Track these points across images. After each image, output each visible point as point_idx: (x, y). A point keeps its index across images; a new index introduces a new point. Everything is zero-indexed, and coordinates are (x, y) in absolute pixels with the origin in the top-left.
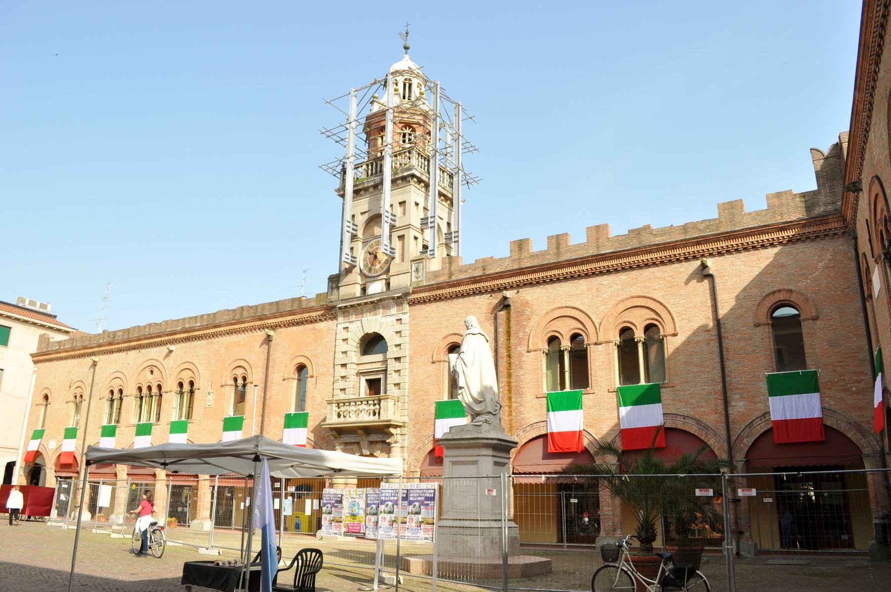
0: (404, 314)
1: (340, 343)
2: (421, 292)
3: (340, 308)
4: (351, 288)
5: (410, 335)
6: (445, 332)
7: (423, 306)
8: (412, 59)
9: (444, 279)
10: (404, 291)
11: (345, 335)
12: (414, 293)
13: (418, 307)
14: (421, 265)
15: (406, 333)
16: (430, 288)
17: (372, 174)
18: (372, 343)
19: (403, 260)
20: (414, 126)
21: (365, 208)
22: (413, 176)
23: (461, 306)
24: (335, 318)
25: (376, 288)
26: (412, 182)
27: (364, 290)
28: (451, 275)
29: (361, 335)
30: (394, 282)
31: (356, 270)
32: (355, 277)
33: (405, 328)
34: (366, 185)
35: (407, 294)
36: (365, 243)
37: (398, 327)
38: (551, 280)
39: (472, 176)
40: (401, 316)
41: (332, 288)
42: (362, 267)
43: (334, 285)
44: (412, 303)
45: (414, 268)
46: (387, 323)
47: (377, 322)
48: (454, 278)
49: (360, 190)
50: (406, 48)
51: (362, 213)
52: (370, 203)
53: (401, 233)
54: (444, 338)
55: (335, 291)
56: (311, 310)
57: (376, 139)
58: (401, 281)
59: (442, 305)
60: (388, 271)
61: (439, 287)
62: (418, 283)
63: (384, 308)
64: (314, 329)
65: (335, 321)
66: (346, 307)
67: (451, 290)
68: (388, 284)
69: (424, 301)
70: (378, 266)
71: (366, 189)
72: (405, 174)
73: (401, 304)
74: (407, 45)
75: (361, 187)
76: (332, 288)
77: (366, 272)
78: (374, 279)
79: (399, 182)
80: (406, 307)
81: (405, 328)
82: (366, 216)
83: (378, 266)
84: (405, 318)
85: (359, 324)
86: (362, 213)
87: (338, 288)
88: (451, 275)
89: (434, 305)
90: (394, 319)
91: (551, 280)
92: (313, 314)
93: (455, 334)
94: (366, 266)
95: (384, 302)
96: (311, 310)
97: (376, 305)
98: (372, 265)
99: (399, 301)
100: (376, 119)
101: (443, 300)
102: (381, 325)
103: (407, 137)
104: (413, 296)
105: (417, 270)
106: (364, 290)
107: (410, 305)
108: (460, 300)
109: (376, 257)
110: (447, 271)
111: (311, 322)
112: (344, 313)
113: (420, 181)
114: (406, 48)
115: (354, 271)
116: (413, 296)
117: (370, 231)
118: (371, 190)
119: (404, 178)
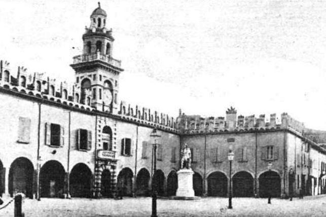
18: (107, 130)
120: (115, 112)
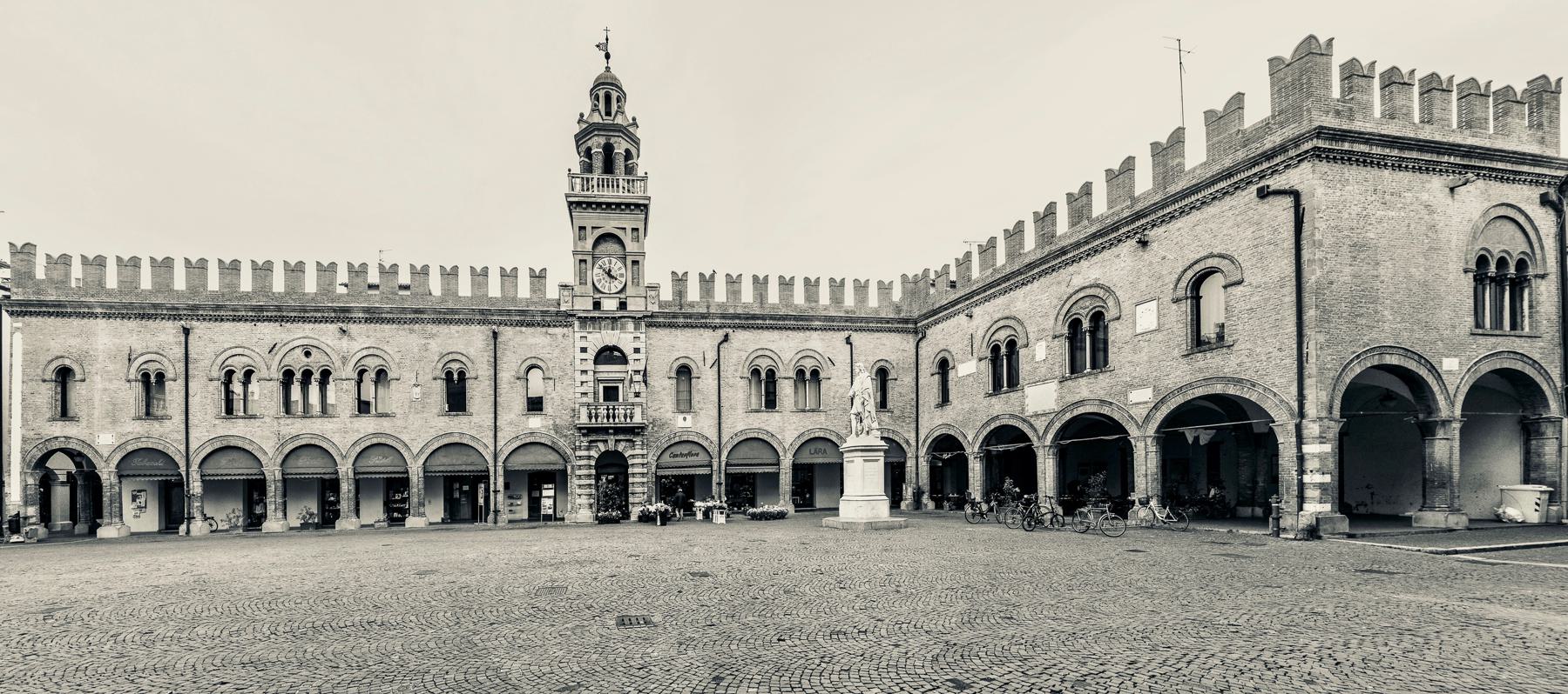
47: (624, 338)
120: (635, 306)
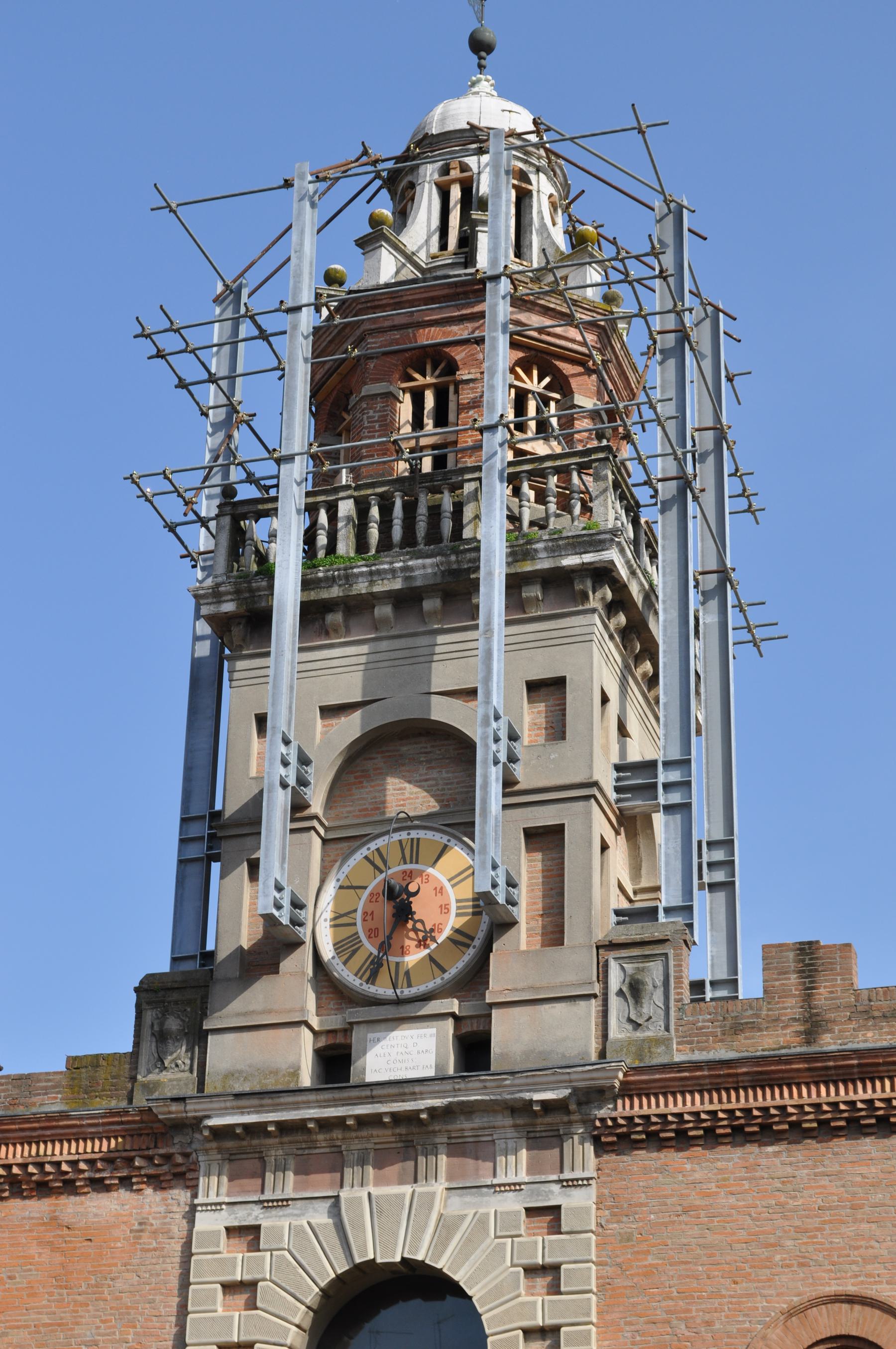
0: (568, 1184)
1: (584, 1272)
2: (666, 1090)
3: (219, 1133)
4: (265, 1045)
5: (604, 1285)
6: (798, 1287)
7: (671, 1157)
8: (503, 92)
9: (778, 1039)
10: (581, 1078)
11: (239, 1263)
12: (628, 1091)
13: (642, 1160)
14: (655, 970)
15: (584, 1272)
16: (719, 1077)
17: (385, 544)
19: (554, 934)
20: (567, 368)
21: (350, 687)
22: (603, 574)
23: (872, 1171)
24: (183, 1175)
25: (406, 1054)
26: (594, 602)
27: (335, 1062)
28: (813, 1025)
29: (330, 1267)
30: (508, 1035)
31: (298, 964)
32: (292, 989)
33: (580, 1255)
34: (361, 587)
35: (592, 1095)
36: (338, 845)
37: (541, 1247)
38: (766, 1128)
39: (755, 616)
40: (555, 1196)
41: (162, 1037)
42: (327, 952)
43: (173, 1024)
44: (615, 1140)
45: (615, 979)
46: (482, 1222)
48: (829, 1043)
49: (328, 606)
50: (480, 46)
51: (328, 711)
52: (369, 667)
53: (544, 817)
54: (791, 1313)
55: (180, 1054)
56: (51, 1128)
57: (391, 398)
58: (546, 1032)
59: (773, 1159)
60: (475, 978)
61: (767, 1073)
62: (641, 1048)
63: (459, 1148)
64: (54, 1220)
65: (181, 1195)
66: (250, 1129)
67: (824, 1094)
68: (473, 1049)
69: (678, 1136)
70: (414, 957)
71: (357, 608)
72: (571, 561)
73: (557, 1139)
74: (489, 34)
75: (335, 592)
76: (162, 1037)
77: (346, 974)
78: (402, 1011)
79: (534, 591)
80: (583, 1157)
81: (580, 1255)
82: (351, 727)
83: (414, 957)
84: (578, 1203)
85: (320, 1216)
86: (328, 711)
87: (198, 1038)
88: (813, 1025)
89: (730, 1159)
90: (514, 1204)
91: (766, 1128)
92: (61, 1152)
93: (851, 1300)
94: (346, 947)
95: (465, 1125)
96: (51, 1128)
97: (409, 1134)
98: (385, 947)
99: (542, 1126)
100: (400, 315)
101: (777, 1137)
102: (447, 1227)
103: (532, 407)
104: (623, 1109)
105: (635, 990)
106: (335, 1062)
107: (601, 1148)
108: (868, 1145)
109: (403, 912)
110: (792, 1007)
111: (43, 1189)
112: (231, 1157)
113: (620, 601)
114: (480, 46)
115: (287, 965)
116: (623, 1109)
117: (364, 794)
118: (384, 610)
119: (559, 583)
